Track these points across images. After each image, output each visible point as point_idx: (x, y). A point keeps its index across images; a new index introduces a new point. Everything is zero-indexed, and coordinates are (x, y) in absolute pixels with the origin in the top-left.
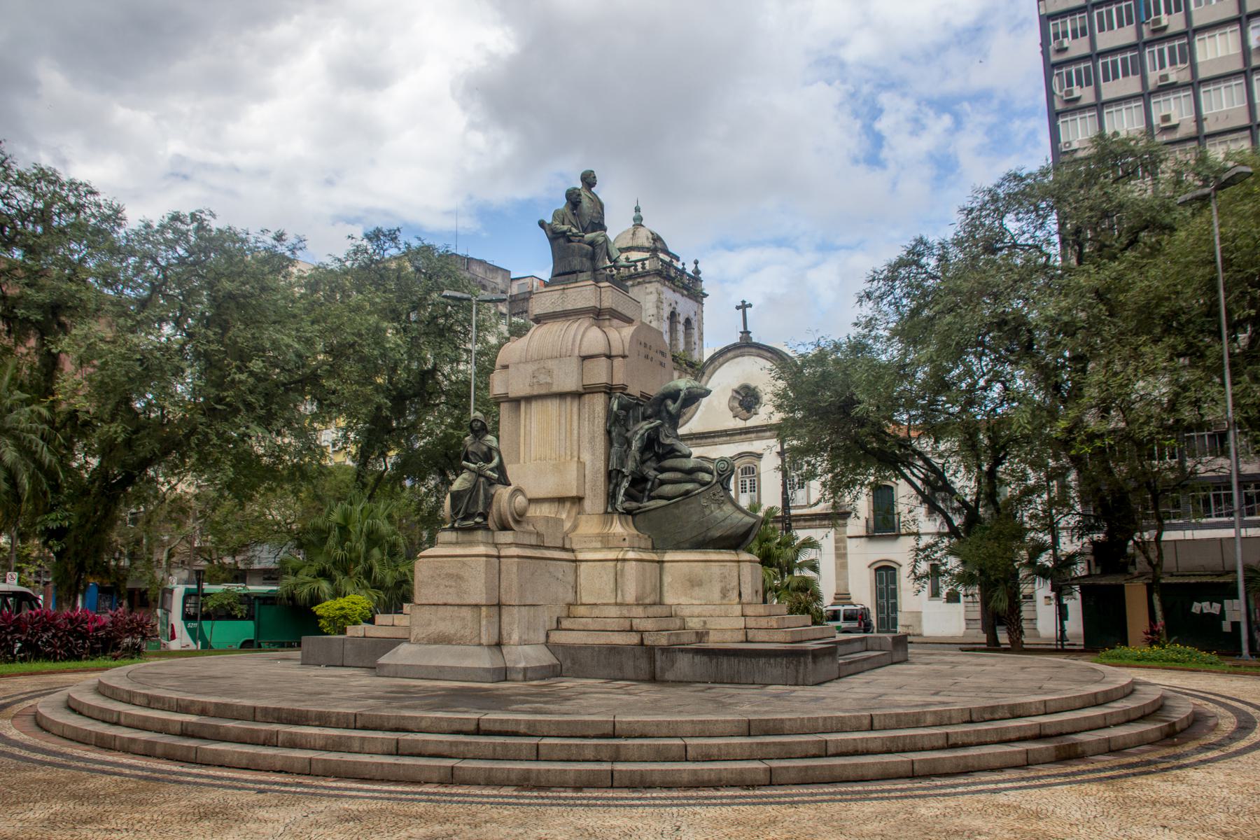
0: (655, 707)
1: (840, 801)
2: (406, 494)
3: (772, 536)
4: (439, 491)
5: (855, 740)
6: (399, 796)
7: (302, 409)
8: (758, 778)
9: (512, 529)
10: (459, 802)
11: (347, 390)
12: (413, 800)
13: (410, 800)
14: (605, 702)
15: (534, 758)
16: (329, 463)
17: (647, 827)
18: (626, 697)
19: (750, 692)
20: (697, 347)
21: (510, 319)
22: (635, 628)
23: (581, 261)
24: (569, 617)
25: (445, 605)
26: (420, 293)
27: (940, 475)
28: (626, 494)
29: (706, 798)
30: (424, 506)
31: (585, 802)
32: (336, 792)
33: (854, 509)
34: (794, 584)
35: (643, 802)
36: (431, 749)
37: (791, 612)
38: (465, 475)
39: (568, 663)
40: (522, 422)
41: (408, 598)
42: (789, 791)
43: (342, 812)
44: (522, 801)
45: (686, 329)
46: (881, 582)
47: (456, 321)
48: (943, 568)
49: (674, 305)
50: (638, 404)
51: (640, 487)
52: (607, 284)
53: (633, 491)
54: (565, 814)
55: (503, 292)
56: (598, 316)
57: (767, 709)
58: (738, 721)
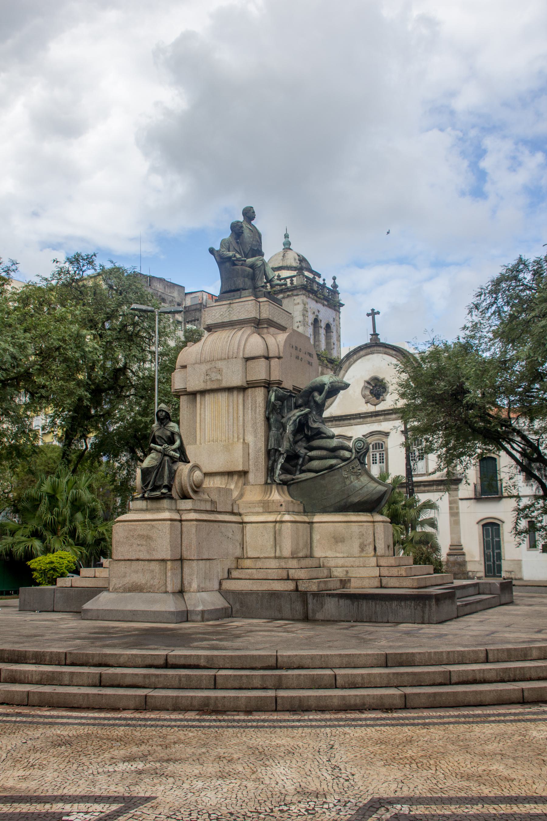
0: (309, 643)
1: (464, 723)
2: (103, 468)
3: (399, 499)
4: (129, 466)
5: (473, 670)
6: (102, 722)
7: (17, 400)
8: (395, 702)
9: (191, 498)
10: (152, 726)
11: (54, 385)
12: (114, 725)
13: (111, 725)
14: (268, 639)
15: (212, 687)
16: (40, 443)
17: (306, 746)
18: (285, 634)
19: (385, 630)
20: (335, 346)
21: (185, 326)
22: (291, 577)
23: (244, 281)
24: (237, 568)
25: (138, 560)
26: (113, 307)
27: (536, 449)
28: (282, 468)
29: (354, 720)
30: (118, 477)
31: (255, 724)
32: (50, 720)
33: (465, 477)
34: (417, 538)
35: (302, 724)
36: (128, 681)
37: (415, 563)
38: (153, 455)
39: (237, 606)
40: (198, 411)
41: (106, 553)
42: (420, 714)
43: (55, 737)
44: (203, 724)
45: (327, 332)
46: (488, 536)
47: (142, 328)
48: (539, 525)
49: (316, 313)
50: (291, 396)
51: (293, 463)
52: (265, 299)
53: (288, 466)
54: (239, 735)
55: (179, 305)
56: (258, 325)
57: (400, 644)
58: (378, 654)
